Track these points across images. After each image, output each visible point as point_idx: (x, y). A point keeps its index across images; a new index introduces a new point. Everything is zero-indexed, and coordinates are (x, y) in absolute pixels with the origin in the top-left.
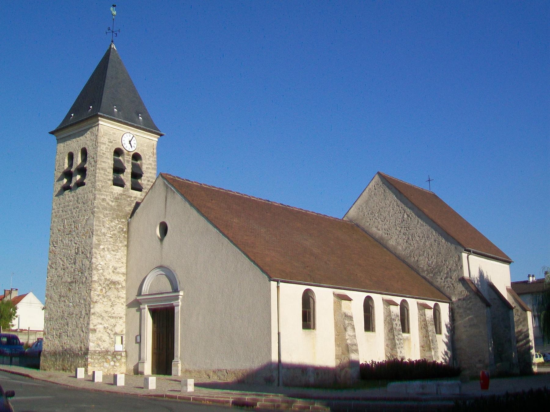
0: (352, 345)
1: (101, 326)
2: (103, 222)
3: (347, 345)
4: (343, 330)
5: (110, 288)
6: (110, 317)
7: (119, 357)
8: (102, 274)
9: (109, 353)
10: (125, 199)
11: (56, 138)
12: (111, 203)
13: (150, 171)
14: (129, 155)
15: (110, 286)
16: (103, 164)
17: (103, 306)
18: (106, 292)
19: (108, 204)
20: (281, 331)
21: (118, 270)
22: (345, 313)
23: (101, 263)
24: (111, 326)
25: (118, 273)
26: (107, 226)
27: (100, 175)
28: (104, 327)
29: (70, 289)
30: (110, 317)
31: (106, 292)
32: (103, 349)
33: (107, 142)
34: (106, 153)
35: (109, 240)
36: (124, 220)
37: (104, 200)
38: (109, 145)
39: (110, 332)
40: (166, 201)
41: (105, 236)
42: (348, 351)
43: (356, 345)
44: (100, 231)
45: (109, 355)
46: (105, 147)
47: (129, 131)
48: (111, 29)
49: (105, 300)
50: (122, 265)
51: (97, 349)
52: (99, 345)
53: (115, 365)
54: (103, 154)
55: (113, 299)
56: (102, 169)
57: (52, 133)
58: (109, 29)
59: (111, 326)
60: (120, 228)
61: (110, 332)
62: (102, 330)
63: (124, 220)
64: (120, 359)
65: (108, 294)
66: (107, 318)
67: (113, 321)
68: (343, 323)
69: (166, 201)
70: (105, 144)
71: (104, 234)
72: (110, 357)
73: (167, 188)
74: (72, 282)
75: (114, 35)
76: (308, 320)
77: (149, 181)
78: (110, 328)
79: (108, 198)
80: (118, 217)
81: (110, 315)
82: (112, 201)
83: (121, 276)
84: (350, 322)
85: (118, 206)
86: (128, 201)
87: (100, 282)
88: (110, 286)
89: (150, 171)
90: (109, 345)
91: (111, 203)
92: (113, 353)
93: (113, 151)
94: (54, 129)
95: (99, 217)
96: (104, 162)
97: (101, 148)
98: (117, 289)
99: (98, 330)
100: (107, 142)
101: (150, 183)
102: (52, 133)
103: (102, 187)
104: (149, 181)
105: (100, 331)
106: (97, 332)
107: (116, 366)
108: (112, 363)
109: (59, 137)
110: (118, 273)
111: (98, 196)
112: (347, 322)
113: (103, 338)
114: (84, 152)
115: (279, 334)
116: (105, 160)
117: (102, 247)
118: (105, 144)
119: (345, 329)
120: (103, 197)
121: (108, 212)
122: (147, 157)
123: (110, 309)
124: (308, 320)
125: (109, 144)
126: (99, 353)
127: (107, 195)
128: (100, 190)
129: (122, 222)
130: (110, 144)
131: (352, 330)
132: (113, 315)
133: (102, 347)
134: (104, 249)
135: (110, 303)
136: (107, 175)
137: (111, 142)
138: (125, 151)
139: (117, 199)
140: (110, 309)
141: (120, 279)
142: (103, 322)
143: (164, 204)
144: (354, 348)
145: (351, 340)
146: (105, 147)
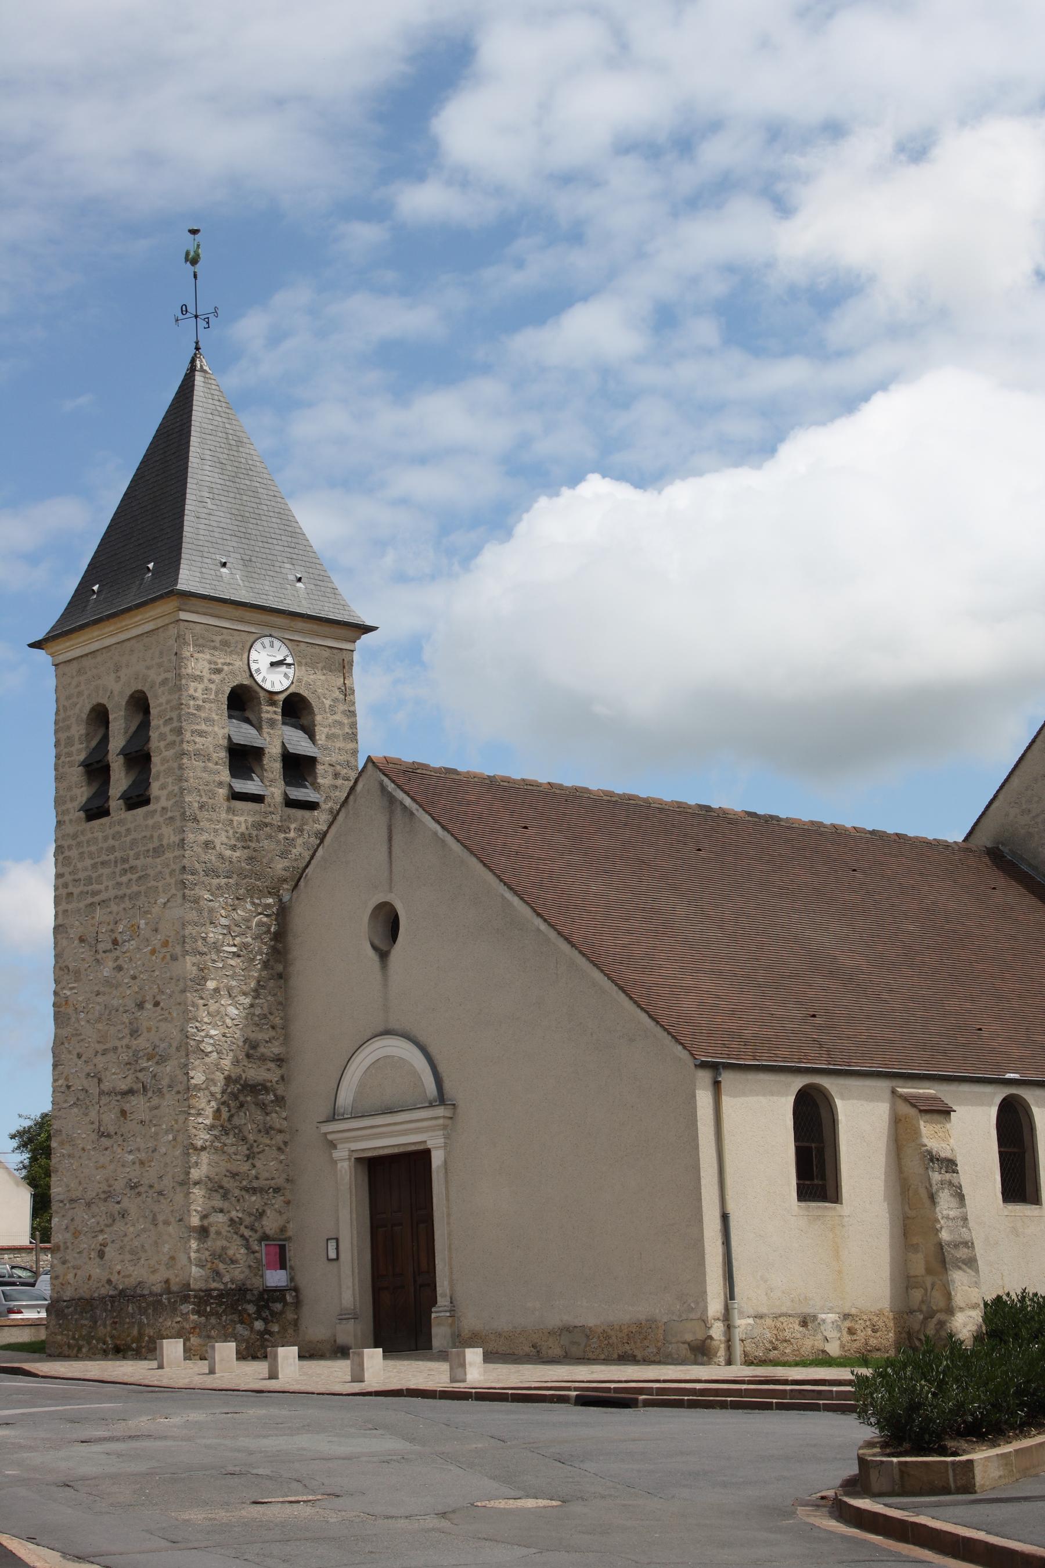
0: (956, 1246)
1: (221, 1218)
2: (211, 911)
3: (940, 1246)
4: (927, 1201)
5: (242, 1105)
6: (246, 1189)
7: (278, 1307)
8: (217, 1065)
9: (248, 1297)
10: (270, 837)
11: (49, 659)
12: (228, 853)
13: (339, 744)
14: (273, 703)
15: (241, 1098)
16: (198, 739)
17: (225, 1157)
18: (231, 1117)
19: (221, 856)
20: (731, 1208)
21: (262, 1050)
22: (930, 1152)
23: (213, 1032)
24: (250, 1214)
25: (263, 1059)
26: (224, 921)
27: (195, 772)
28: (231, 1220)
29: (123, 1113)
30: (246, 1189)
31: (231, 1117)
32: (229, 1286)
33: (206, 674)
34: (207, 705)
35: (232, 962)
36: (270, 901)
37: (208, 845)
38: (211, 681)
39: (247, 1233)
40: (390, 839)
41: (219, 951)
42: (943, 1262)
43: (969, 1244)
44: (204, 939)
45: (249, 1302)
46: (201, 687)
47: (267, 632)
48: (191, 309)
49: (230, 1140)
50: (272, 1033)
51: (214, 1285)
52: (217, 1273)
53: (267, 1331)
54: (199, 708)
55: (251, 1137)
56: (197, 754)
57: (36, 645)
58: (184, 310)
59: (250, 1214)
60: (260, 924)
61: (247, 1233)
62: (225, 1230)
63: (270, 901)
64: (282, 1312)
65: (236, 1121)
66: (237, 1192)
67: (254, 1201)
68: (918, 1182)
69: (390, 839)
70: (199, 678)
71: (216, 947)
72: (251, 1309)
73: (391, 813)
74: (131, 1092)
75: (202, 324)
76: (817, 1173)
77: (336, 776)
78: (248, 1220)
79: (220, 840)
80: (251, 891)
81: (244, 1183)
82: (233, 848)
83: (272, 1065)
84: (948, 1176)
85: (251, 859)
86: (278, 842)
87: (212, 1089)
88: (241, 1098)
89: (339, 744)
90: (247, 1271)
91: (228, 853)
92: (261, 1294)
93: (224, 699)
94: (40, 637)
95: (196, 901)
96: (201, 734)
97: (191, 692)
98: (263, 1107)
99: (213, 1230)
100: (206, 674)
101: (339, 782)
102: (36, 645)
103: (201, 807)
104: (336, 776)
105: (218, 1233)
106: (212, 1235)
107: (271, 1333)
108: (259, 1325)
109: (62, 658)
110: (263, 1059)
111: (190, 837)
112: (936, 1177)
113: (230, 1252)
114: (140, 703)
115: (725, 1218)
116: (203, 727)
117: (211, 985)
118: (199, 678)
119: (932, 1198)
120: (205, 837)
121: (223, 881)
122: (328, 703)
123: (245, 1167)
124: (817, 1173)
125: (213, 677)
126: (221, 1296)
127: (216, 831)
128: (196, 820)
129: (268, 906)
130: (216, 677)
131: (954, 1202)
132: (255, 1184)
133: (226, 1279)
134: (217, 990)
135: (243, 1149)
136: (211, 772)
137: (218, 671)
138: (262, 694)
139: (245, 839)
140: (245, 1167)
141: (268, 1076)
142: (226, 1205)
143: (384, 848)
144: (962, 1253)
145: (951, 1232)
146: (201, 687)
